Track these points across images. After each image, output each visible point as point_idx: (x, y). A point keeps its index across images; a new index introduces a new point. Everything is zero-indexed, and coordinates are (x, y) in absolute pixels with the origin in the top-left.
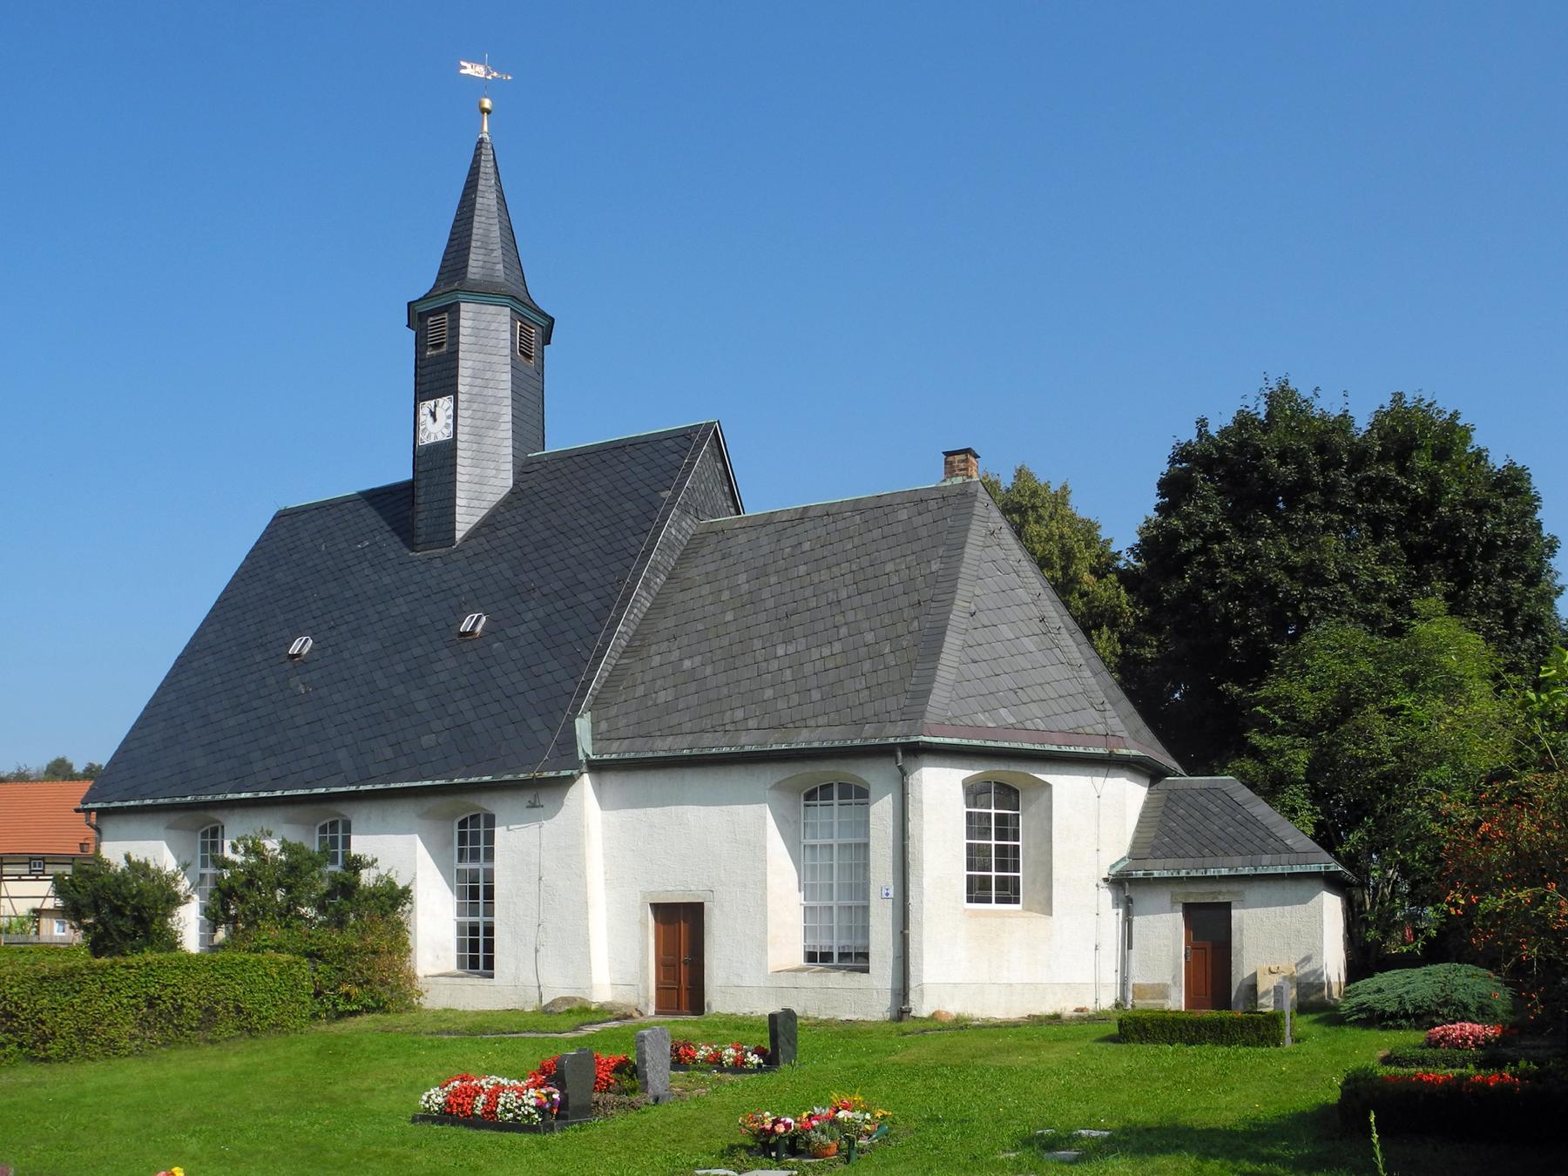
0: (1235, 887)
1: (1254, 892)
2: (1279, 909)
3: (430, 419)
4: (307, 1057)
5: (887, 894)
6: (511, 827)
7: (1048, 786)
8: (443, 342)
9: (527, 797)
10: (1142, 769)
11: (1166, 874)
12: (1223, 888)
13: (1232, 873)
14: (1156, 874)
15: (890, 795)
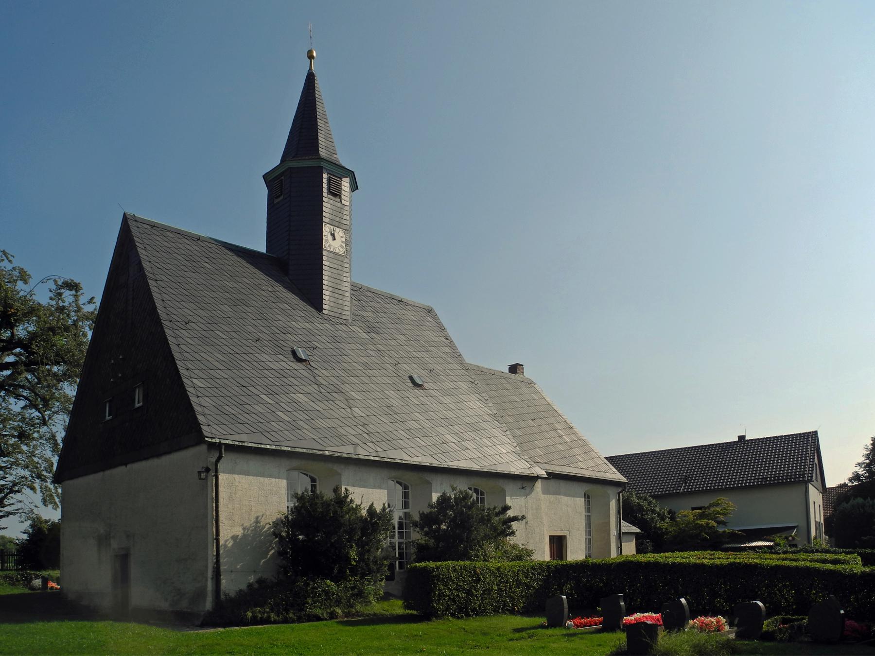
3: (330, 238)
6: (513, 498)
8: (338, 195)
9: (519, 484)
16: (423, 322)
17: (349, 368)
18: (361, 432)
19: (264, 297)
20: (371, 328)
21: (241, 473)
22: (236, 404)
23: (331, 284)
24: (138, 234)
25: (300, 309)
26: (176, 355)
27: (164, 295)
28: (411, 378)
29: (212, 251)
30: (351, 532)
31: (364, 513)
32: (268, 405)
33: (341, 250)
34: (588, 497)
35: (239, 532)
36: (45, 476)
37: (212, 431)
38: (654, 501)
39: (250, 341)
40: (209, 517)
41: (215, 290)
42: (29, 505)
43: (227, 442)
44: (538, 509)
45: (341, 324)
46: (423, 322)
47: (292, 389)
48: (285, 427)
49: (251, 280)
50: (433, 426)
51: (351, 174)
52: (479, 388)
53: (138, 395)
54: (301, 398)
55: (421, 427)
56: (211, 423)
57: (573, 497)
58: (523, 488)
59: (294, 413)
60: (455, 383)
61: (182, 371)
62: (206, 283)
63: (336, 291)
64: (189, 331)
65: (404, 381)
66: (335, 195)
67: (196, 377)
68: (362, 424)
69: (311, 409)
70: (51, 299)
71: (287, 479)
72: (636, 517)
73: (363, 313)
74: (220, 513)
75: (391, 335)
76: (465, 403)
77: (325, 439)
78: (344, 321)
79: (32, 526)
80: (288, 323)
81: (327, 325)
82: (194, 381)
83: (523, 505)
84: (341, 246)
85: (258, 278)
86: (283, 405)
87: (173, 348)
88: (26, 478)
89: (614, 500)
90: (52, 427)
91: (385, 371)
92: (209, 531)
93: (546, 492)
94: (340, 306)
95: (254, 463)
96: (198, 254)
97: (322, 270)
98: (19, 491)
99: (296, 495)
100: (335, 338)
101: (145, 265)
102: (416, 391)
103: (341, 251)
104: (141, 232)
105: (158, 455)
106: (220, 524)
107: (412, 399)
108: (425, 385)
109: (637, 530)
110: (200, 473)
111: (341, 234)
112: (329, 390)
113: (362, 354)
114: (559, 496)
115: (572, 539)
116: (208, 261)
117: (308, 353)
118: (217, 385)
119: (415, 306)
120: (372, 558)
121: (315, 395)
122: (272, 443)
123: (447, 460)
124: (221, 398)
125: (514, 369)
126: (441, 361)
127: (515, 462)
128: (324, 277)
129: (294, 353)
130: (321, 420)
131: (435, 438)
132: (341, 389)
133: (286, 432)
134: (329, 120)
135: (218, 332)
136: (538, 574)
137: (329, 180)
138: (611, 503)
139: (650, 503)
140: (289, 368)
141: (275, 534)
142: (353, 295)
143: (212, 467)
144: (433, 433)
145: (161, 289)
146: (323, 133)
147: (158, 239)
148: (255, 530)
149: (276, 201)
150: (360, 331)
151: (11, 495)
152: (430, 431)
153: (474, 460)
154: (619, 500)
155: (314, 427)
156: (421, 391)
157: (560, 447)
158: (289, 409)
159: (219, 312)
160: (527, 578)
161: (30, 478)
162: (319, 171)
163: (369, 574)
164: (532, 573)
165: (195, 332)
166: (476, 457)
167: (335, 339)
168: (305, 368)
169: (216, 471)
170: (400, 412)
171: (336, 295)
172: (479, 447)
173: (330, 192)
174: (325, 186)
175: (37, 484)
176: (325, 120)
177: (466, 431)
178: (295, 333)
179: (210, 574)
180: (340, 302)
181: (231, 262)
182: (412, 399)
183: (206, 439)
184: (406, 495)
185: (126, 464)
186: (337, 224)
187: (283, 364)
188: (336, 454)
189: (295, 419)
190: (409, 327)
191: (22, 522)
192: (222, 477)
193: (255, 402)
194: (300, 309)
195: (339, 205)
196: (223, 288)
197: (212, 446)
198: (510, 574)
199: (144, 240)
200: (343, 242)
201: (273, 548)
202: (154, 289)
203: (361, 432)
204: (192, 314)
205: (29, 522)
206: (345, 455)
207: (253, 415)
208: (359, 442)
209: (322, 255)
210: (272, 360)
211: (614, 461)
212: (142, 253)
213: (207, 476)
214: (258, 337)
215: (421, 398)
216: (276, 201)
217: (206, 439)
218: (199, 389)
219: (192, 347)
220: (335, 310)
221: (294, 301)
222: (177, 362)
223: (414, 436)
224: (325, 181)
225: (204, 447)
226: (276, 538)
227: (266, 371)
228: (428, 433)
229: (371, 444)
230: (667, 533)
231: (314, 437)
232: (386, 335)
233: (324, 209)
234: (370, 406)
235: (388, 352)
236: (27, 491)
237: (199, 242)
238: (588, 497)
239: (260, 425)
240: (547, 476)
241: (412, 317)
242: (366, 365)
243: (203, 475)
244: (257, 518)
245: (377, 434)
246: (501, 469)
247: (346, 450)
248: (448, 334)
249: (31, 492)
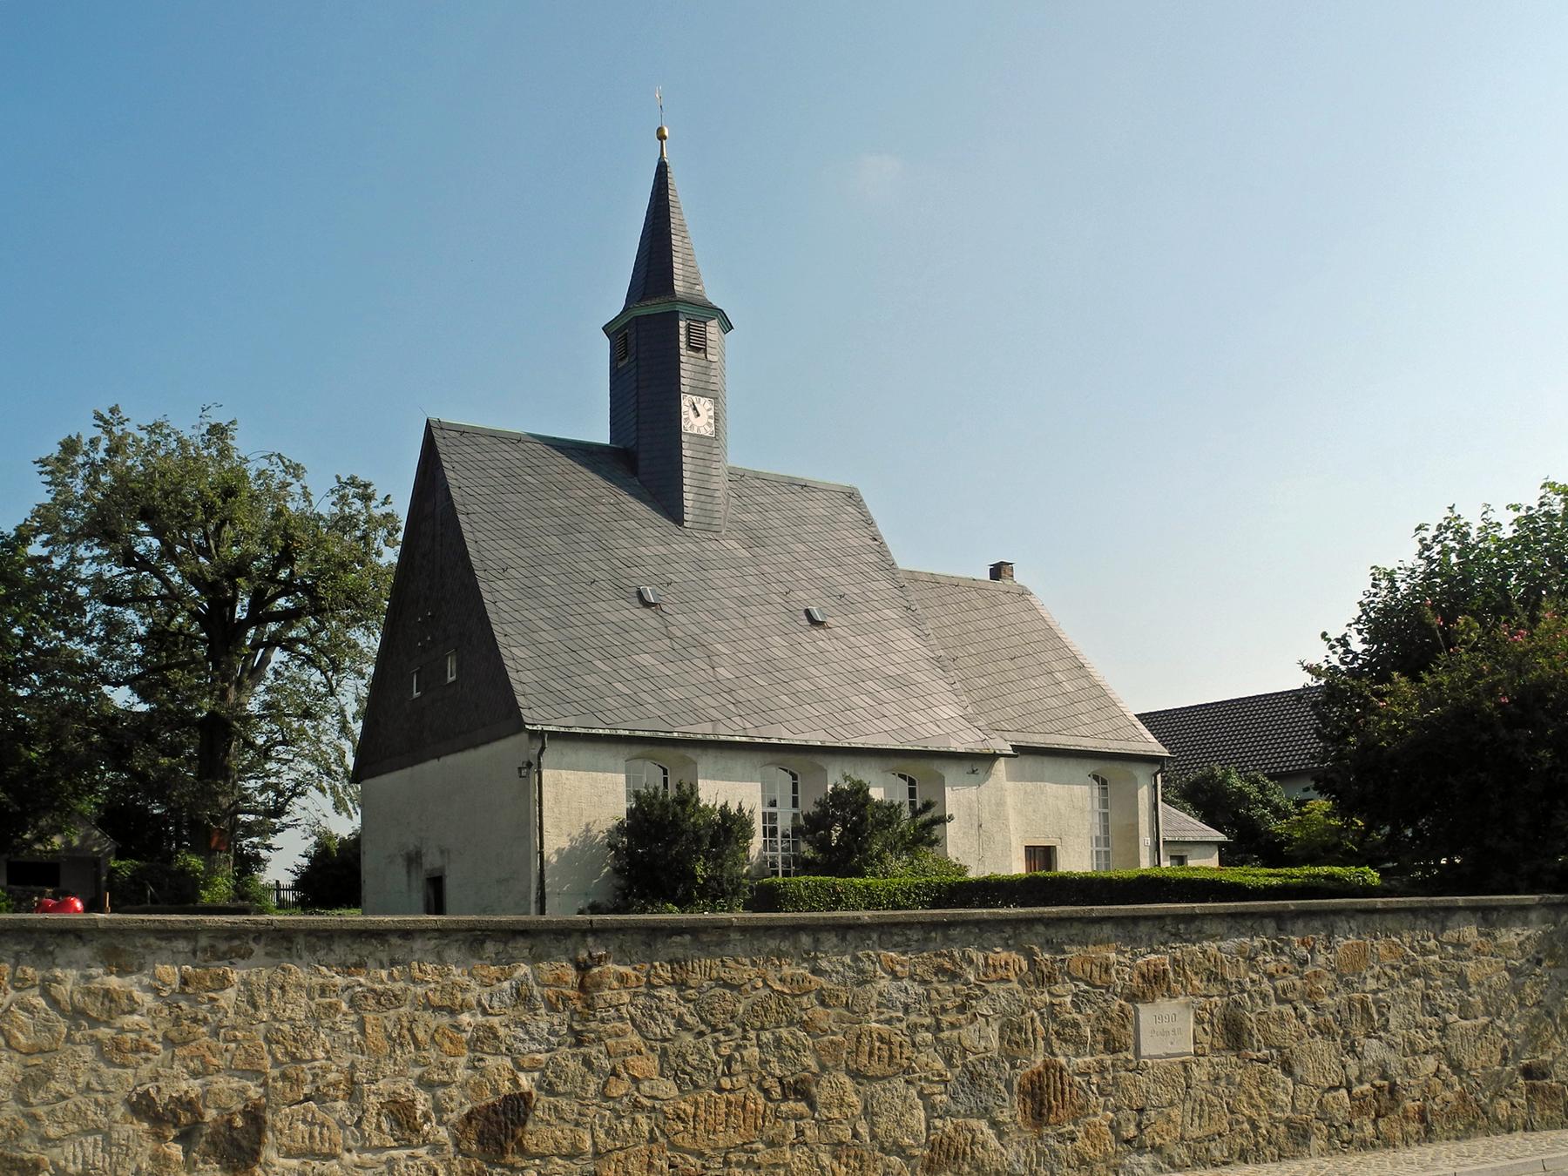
0: (1189, 848)
1: (1197, 850)
3: (691, 413)
7: (1136, 778)
9: (967, 766)
11: (1171, 839)
12: (1184, 848)
16: (839, 517)
17: (716, 607)
18: (724, 702)
19: (603, 516)
20: (754, 539)
21: (568, 769)
22: (563, 676)
23: (696, 483)
24: (445, 448)
25: (653, 525)
26: (492, 617)
27: (477, 534)
28: (808, 613)
29: (537, 456)
30: (698, 839)
31: (717, 817)
32: (603, 675)
33: (708, 429)
34: (1104, 782)
35: (565, 843)
36: (335, 772)
37: (535, 715)
38: (1271, 784)
39: (583, 585)
40: (532, 824)
41: (540, 515)
42: (314, 813)
43: (551, 728)
44: (1001, 804)
45: (710, 539)
46: (839, 517)
47: (635, 649)
48: (624, 703)
49: (587, 491)
50: (834, 685)
51: (719, 314)
52: (918, 617)
53: (451, 665)
54: (645, 660)
55: (814, 688)
56: (532, 705)
57: (1069, 784)
58: (973, 772)
59: (637, 682)
60: (878, 612)
61: (500, 639)
62: (529, 507)
63: (702, 491)
64: (507, 581)
65: (795, 618)
66: (697, 350)
67: (516, 644)
68: (727, 690)
69: (659, 674)
70: (333, 504)
71: (627, 772)
72: (1236, 814)
73: (744, 517)
74: (545, 819)
75: (784, 546)
76: (891, 643)
77: (674, 717)
78: (714, 535)
79: (316, 844)
80: (634, 550)
81: (689, 545)
82: (513, 650)
83: (974, 798)
84: (709, 424)
85: (596, 485)
86: (622, 672)
87: (489, 607)
88: (312, 775)
89: (1145, 787)
90: (340, 697)
91: (769, 607)
92: (532, 842)
93: (1013, 777)
94: (708, 513)
95: (584, 753)
96: (519, 464)
97: (682, 462)
98: (303, 794)
99: (637, 795)
100: (699, 563)
101: (454, 493)
102: (814, 632)
103: (707, 431)
104: (449, 444)
105: (475, 746)
106: (545, 833)
107: (807, 646)
108: (829, 620)
109: (1222, 837)
110: (520, 768)
111: (708, 405)
112: (685, 645)
113: (737, 584)
114: (1042, 784)
115: (1066, 852)
116: (531, 472)
117: (659, 591)
118: (541, 654)
119: (827, 491)
120: (725, 875)
121: (665, 654)
122: (605, 726)
123: (849, 736)
124: (545, 671)
125: (998, 571)
126: (860, 578)
127: (961, 733)
128: (685, 474)
129: (640, 594)
130: (671, 690)
131: (835, 703)
132: (702, 641)
133: (623, 710)
134: (690, 234)
135: (543, 578)
136: (923, 895)
137: (688, 328)
138: (1140, 792)
139: (1262, 789)
140: (634, 618)
141: (611, 846)
142: (731, 489)
143: (534, 762)
144: (832, 696)
145: (474, 525)
146: (680, 255)
147: (470, 451)
148: (584, 841)
149: (621, 364)
150: (737, 546)
151: (294, 799)
152: (828, 693)
153: (892, 733)
154: (1155, 786)
155: (662, 700)
156: (822, 631)
157: (1054, 702)
158: (630, 678)
159: (544, 547)
160: (908, 899)
161: (317, 774)
162: (673, 318)
163: (722, 897)
164: (916, 894)
165: (515, 581)
166: (895, 727)
167: (700, 565)
168: (654, 615)
169: (539, 764)
170: (784, 668)
171: (703, 498)
172: (903, 712)
173: (690, 347)
174: (682, 338)
175: (326, 782)
176: (683, 234)
177: (886, 687)
178: (644, 563)
179: (533, 897)
180: (709, 507)
181: (562, 467)
182: (807, 646)
183: (527, 727)
184: (795, 787)
185: (438, 758)
186: (701, 392)
187: (626, 612)
188: (688, 735)
189: (637, 690)
190: (815, 528)
191: (306, 838)
192: (545, 773)
193: (588, 671)
194: (653, 525)
195: (704, 363)
196: (550, 510)
197: (533, 734)
198: (883, 893)
199: (452, 456)
200: (710, 417)
201: (607, 864)
202: (465, 527)
203: (724, 702)
204: (512, 556)
205: (315, 838)
206: (699, 737)
207: (583, 690)
208: (721, 717)
209: (681, 441)
210: (610, 609)
211: (1153, 720)
212: (449, 474)
213: (528, 773)
214: (593, 577)
215: (820, 643)
216: (621, 364)
217: (527, 727)
218: (519, 661)
219: (509, 603)
220: (702, 519)
221: (645, 514)
222: (493, 626)
223: (802, 703)
224: (682, 331)
225: (525, 736)
226: (612, 850)
227: (602, 626)
228: (824, 696)
229: (737, 719)
230: (1290, 840)
231: (660, 714)
232: (777, 547)
233: (682, 373)
234: (741, 662)
235: (776, 575)
236: (312, 792)
237: (520, 444)
238: (1104, 782)
239: (592, 702)
240: (1012, 753)
241: (821, 510)
242: (742, 601)
243: (524, 772)
244: (588, 825)
245: (748, 704)
246: (933, 746)
247: (702, 730)
248: (877, 531)
249: (321, 794)
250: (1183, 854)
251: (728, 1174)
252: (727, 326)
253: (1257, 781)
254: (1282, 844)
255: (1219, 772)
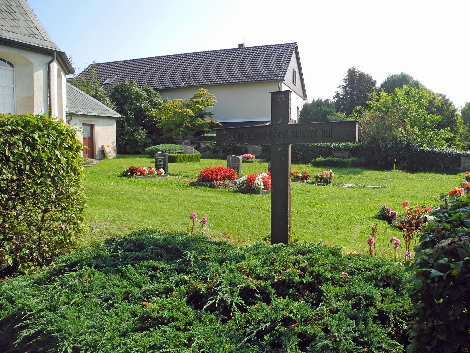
0: (96, 120)
1: (101, 121)
2: (106, 127)
4: (319, 108)
5: (41, 111)
7: (32, 64)
10: (65, 68)
11: (82, 113)
12: (93, 119)
13: (99, 115)
14: (79, 113)
15: (42, 70)
138: (35, 74)
250: (92, 123)
251: (1, 296)
252: (298, 108)
253: (147, 90)
254: (156, 122)
255: (128, 83)
